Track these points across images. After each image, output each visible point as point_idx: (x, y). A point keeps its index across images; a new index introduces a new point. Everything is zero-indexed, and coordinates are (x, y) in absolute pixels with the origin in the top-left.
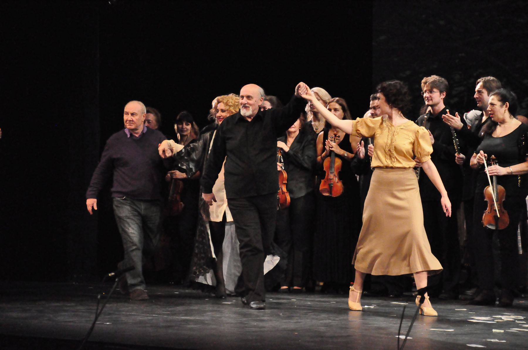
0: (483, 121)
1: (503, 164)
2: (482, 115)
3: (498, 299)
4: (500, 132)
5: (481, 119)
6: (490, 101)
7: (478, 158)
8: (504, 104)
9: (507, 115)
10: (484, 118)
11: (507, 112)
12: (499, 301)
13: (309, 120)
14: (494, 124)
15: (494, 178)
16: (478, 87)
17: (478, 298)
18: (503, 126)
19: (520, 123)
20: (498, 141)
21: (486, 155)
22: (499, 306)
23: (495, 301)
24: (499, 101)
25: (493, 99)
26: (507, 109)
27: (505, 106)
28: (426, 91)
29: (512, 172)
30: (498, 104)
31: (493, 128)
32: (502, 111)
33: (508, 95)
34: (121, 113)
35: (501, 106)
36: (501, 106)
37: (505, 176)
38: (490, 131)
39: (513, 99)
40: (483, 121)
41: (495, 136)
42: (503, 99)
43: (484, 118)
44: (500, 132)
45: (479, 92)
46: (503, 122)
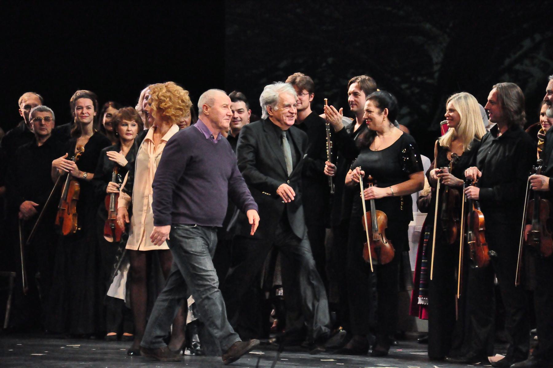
0: (355, 130)
1: (382, 184)
2: (354, 123)
3: (371, 347)
4: (380, 144)
5: (353, 128)
6: (366, 108)
7: (354, 174)
8: (382, 111)
9: (386, 122)
10: (357, 126)
11: (386, 119)
12: (373, 349)
13: (360, 93)
14: (374, 134)
15: (372, 203)
16: (352, 88)
17: (349, 346)
18: (381, 136)
19: (402, 133)
20: (375, 157)
21: (363, 172)
22: (372, 355)
23: (368, 349)
24: (377, 107)
25: (369, 105)
26: (386, 116)
27: (383, 113)
28: (437, 64)
29: (393, 193)
30: (375, 110)
31: (371, 139)
32: (380, 119)
33: (388, 99)
34: (484, 215)
35: (380, 114)
36: (380, 114)
37: (384, 199)
38: (367, 143)
39: (393, 104)
40: (355, 130)
41: (373, 150)
42: (382, 105)
43: (357, 126)
44: (380, 144)
45: (355, 94)
46: (381, 133)
